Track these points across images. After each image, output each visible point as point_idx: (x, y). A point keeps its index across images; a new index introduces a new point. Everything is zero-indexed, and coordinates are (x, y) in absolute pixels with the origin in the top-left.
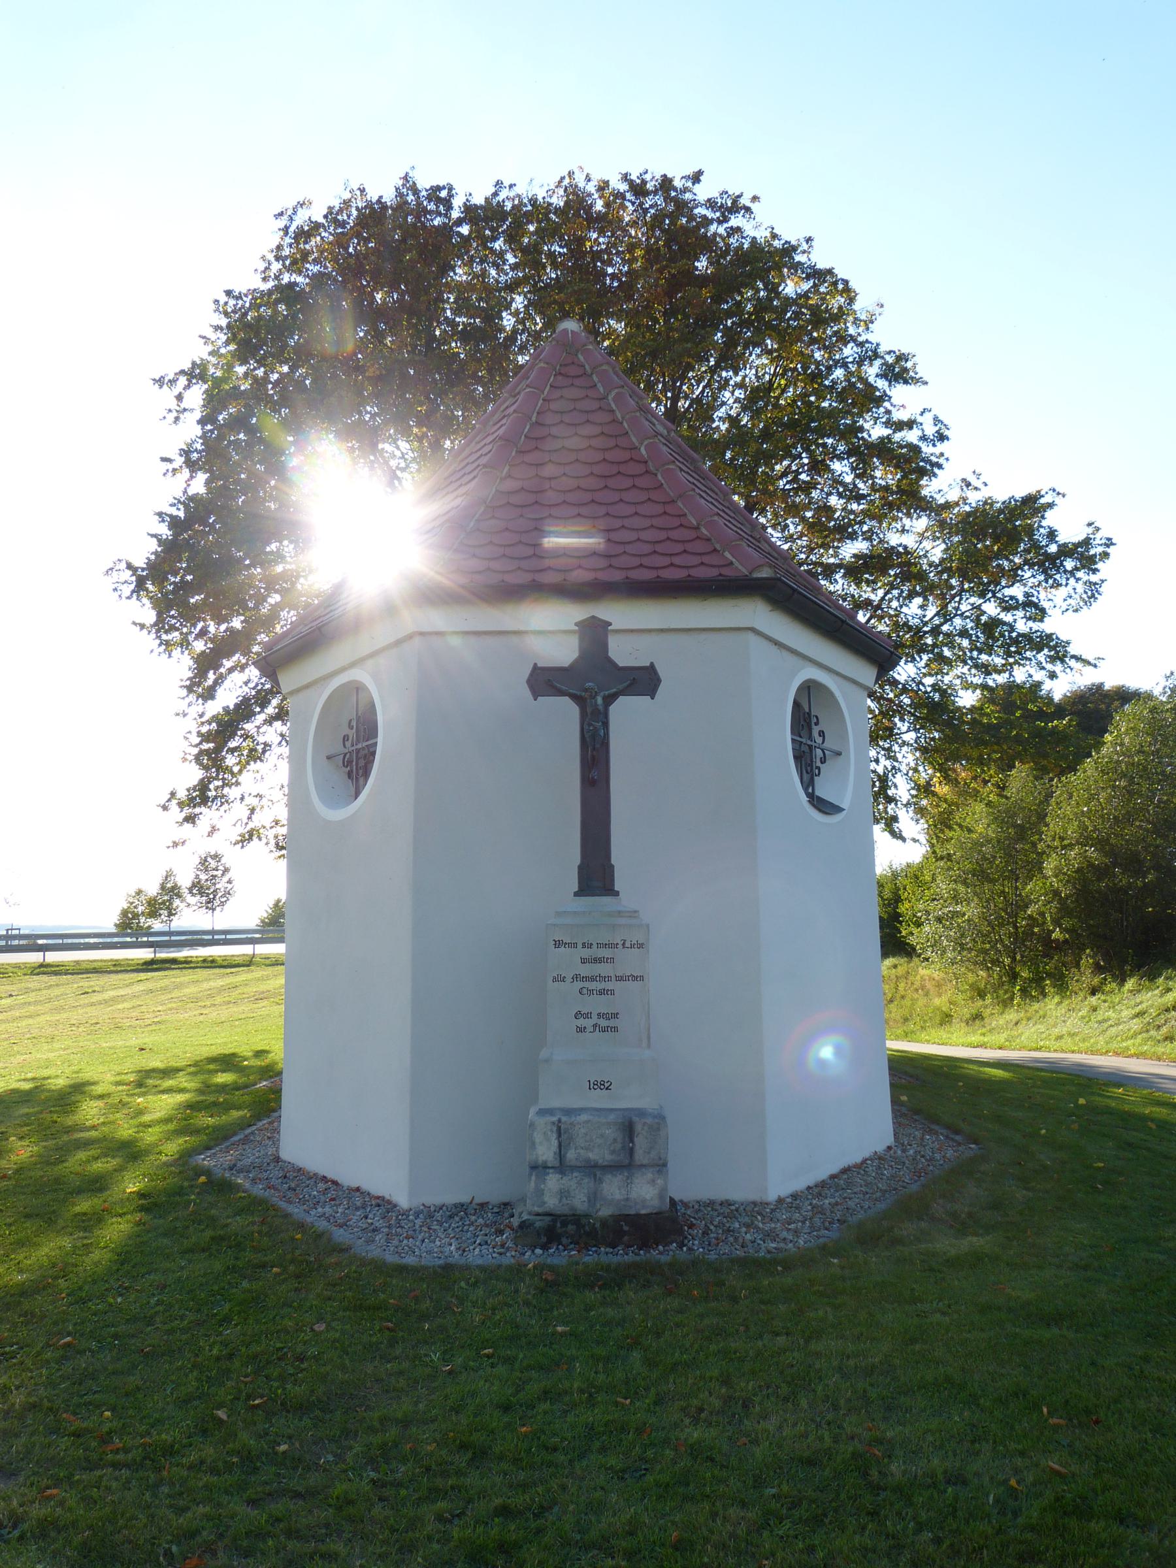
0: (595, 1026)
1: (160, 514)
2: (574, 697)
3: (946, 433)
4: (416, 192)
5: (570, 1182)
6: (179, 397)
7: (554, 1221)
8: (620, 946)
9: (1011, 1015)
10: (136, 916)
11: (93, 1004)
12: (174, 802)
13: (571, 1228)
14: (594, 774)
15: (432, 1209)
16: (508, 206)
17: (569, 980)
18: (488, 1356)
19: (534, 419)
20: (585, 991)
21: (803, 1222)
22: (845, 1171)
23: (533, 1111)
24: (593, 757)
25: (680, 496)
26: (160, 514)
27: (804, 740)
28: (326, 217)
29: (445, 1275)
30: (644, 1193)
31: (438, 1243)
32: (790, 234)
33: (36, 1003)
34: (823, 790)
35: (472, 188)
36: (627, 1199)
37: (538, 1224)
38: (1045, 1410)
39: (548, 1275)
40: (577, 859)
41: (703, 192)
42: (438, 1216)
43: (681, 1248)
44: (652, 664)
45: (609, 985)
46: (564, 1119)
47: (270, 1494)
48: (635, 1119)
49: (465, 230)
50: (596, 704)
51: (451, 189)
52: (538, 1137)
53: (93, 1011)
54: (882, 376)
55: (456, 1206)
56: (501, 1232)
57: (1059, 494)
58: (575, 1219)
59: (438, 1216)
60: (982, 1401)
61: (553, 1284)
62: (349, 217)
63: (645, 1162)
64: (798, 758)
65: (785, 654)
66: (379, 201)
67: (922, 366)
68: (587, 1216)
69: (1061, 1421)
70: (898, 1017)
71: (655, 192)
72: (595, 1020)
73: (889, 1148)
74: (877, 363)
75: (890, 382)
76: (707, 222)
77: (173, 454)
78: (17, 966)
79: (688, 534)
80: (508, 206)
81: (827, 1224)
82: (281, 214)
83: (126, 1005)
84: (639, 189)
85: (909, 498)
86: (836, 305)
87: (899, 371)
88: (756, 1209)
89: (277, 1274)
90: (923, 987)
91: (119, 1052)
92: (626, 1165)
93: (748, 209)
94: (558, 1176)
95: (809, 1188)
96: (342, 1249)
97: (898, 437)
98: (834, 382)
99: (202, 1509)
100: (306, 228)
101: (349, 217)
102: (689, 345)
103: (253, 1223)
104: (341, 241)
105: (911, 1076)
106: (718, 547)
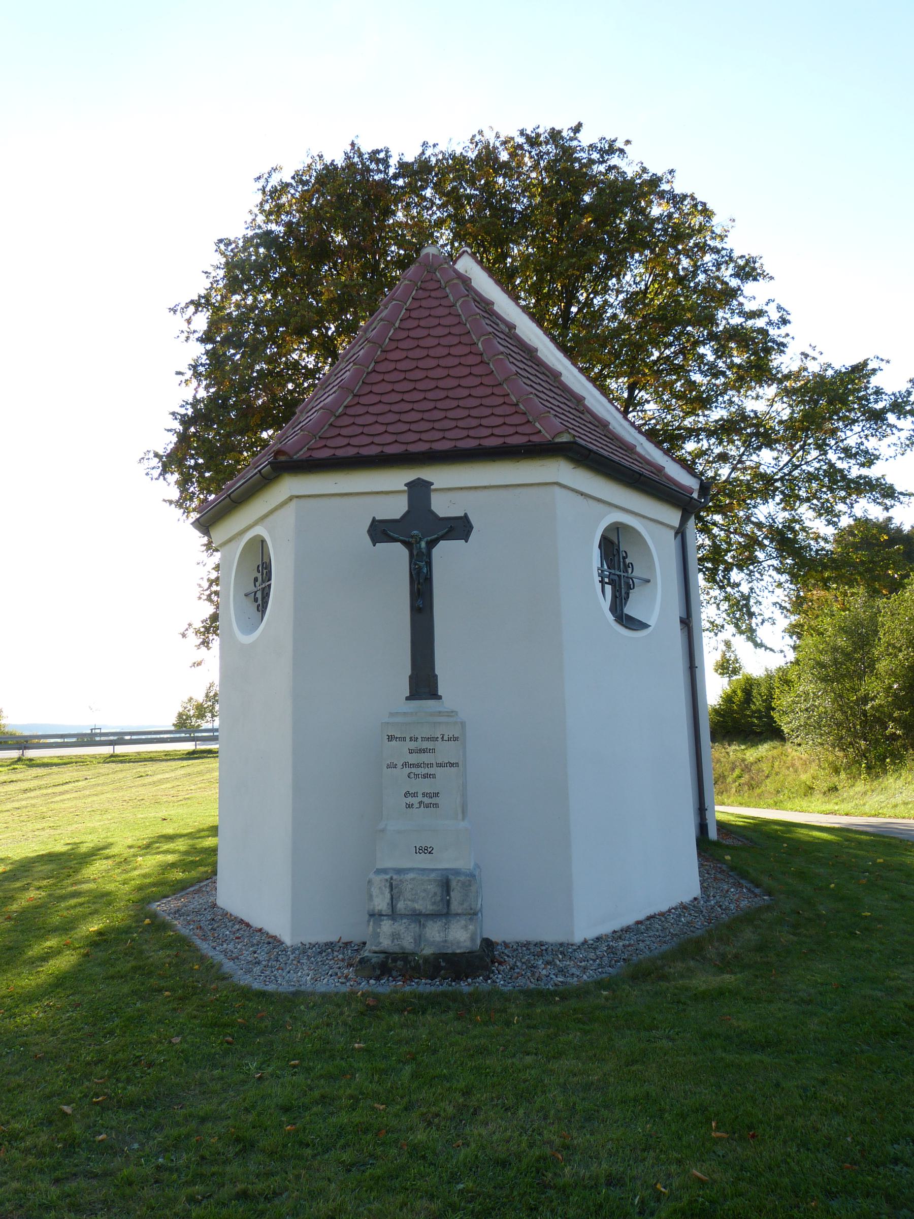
0: (420, 803)
1: (173, 414)
2: (404, 543)
3: (788, 317)
4: (361, 155)
5: (400, 927)
6: (189, 321)
7: (387, 958)
8: (440, 739)
9: (860, 786)
10: (189, 717)
11: (144, 785)
12: (191, 630)
13: (400, 963)
14: (420, 603)
16: (433, 160)
17: (399, 766)
18: (294, 1066)
19: (397, 325)
20: (412, 775)
21: (594, 961)
24: (419, 590)
25: (506, 380)
26: (173, 414)
28: (293, 178)
29: (292, 1000)
30: (459, 937)
31: (299, 974)
32: (657, 168)
33: (103, 784)
34: (630, 610)
35: (405, 150)
36: (446, 941)
37: (374, 960)
38: (713, 1124)
39: (371, 1001)
40: (408, 672)
41: (586, 138)
42: (310, 952)
43: (486, 980)
44: (466, 515)
46: (395, 877)
47: (75, 1175)
48: (451, 877)
49: (400, 182)
50: (420, 547)
51: (387, 152)
52: (375, 891)
53: (142, 791)
54: (736, 275)
55: (326, 944)
57: (882, 360)
58: (404, 956)
59: (310, 952)
60: (666, 1115)
61: (373, 1008)
62: (310, 177)
63: (460, 911)
65: (591, 502)
66: (332, 164)
67: (767, 264)
68: (413, 954)
69: (724, 1135)
70: (772, 790)
71: (547, 143)
73: (695, 899)
74: (732, 265)
75: (742, 280)
76: (592, 162)
77: (184, 368)
78: (94, 757)
79: (509, 410)
80: (433, 160)
82: (259, 178)
83: (169, 785)
84: (534, 141)
85: (759, 371)
86: (697, 223)
87: (748, 271)
88: (564, 949)
89: (168, 997)
90: (793, 765)
91: (125, 823)
92: (444, 913)
93: (622, 151)
94: (390, 922)
96: (224, 978)
97: (750, 323)
98: (697, 284)
99: (15, 1185)
100: (279, 188)
101: (310, 177)
102: (574, 260)
103: (169, 956)
104: (306, 197)
105: (747, 839)
106: (531, 419)
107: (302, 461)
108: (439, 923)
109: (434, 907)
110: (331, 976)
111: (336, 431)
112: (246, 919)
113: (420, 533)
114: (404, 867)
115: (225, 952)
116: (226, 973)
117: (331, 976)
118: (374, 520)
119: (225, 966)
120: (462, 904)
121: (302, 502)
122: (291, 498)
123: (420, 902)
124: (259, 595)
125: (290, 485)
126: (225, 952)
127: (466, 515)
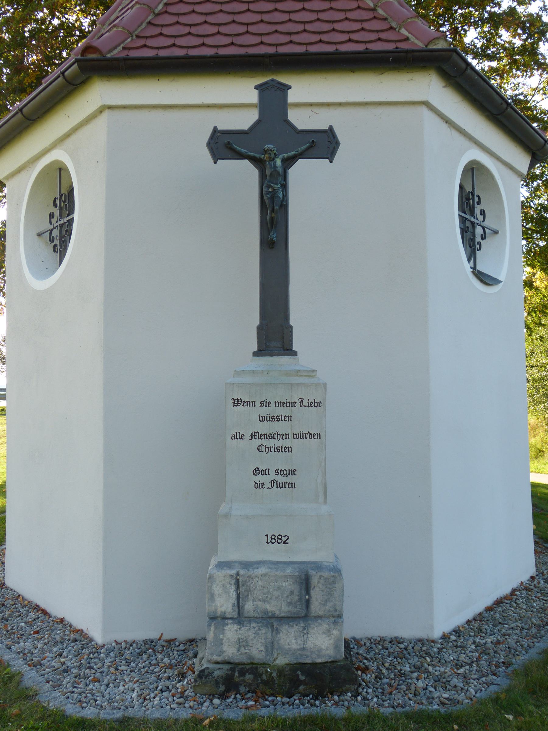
0: (273, 482)
2: (254, 160)
5: (248, 632)
7: (232, 670)
8: (298, 405)
13: (249, 677)
14: (273, 235)
15: (123, 645)
17: (247, 437)
20: (263, 448)
21: (471, 665)
22: (498, 602)
23: (214, 561)
24: (272, 219)
27: (468, 217)
30: (321, 644)
31: (121, 688)
36: (304, 649)
37: (217, 673)
40: (256, 320)
44: (331, 128)
45: (286, 443)
46: (242, 572)
48: (311, 572)
50: (275, 164)
52: (217, 589)
55: (145, 642)
56: (182, 675)
58: (253, 668)
63: (321, 613)
64: (464, 231)
65: (456, 134)
68: (264, 664)
72: (272, 476)
73: (532, 578)
81: (493, 668)
88: (423, 646)
92: (303, 616)
94: (236, 626)
95: (468, 622)
106: (394, 25)
107: (118, 60)
108: (296, 628)
109: (291, 609)
110: (162, 691)
111: (157, 31)
112: (43, 605)
113: (272, 151)
114: (253, 559)
115: (23, 653)
116: (27, 689)
117: (162, 691)
118: (215, 130)
119: (26, 677)
120: (325, 605)
121: (116, 113)
122: (101, 110)
123: (273, 602)
124: (56, 233)
125: (101, 93)
126: (23, 653)
127: (331, 128)
